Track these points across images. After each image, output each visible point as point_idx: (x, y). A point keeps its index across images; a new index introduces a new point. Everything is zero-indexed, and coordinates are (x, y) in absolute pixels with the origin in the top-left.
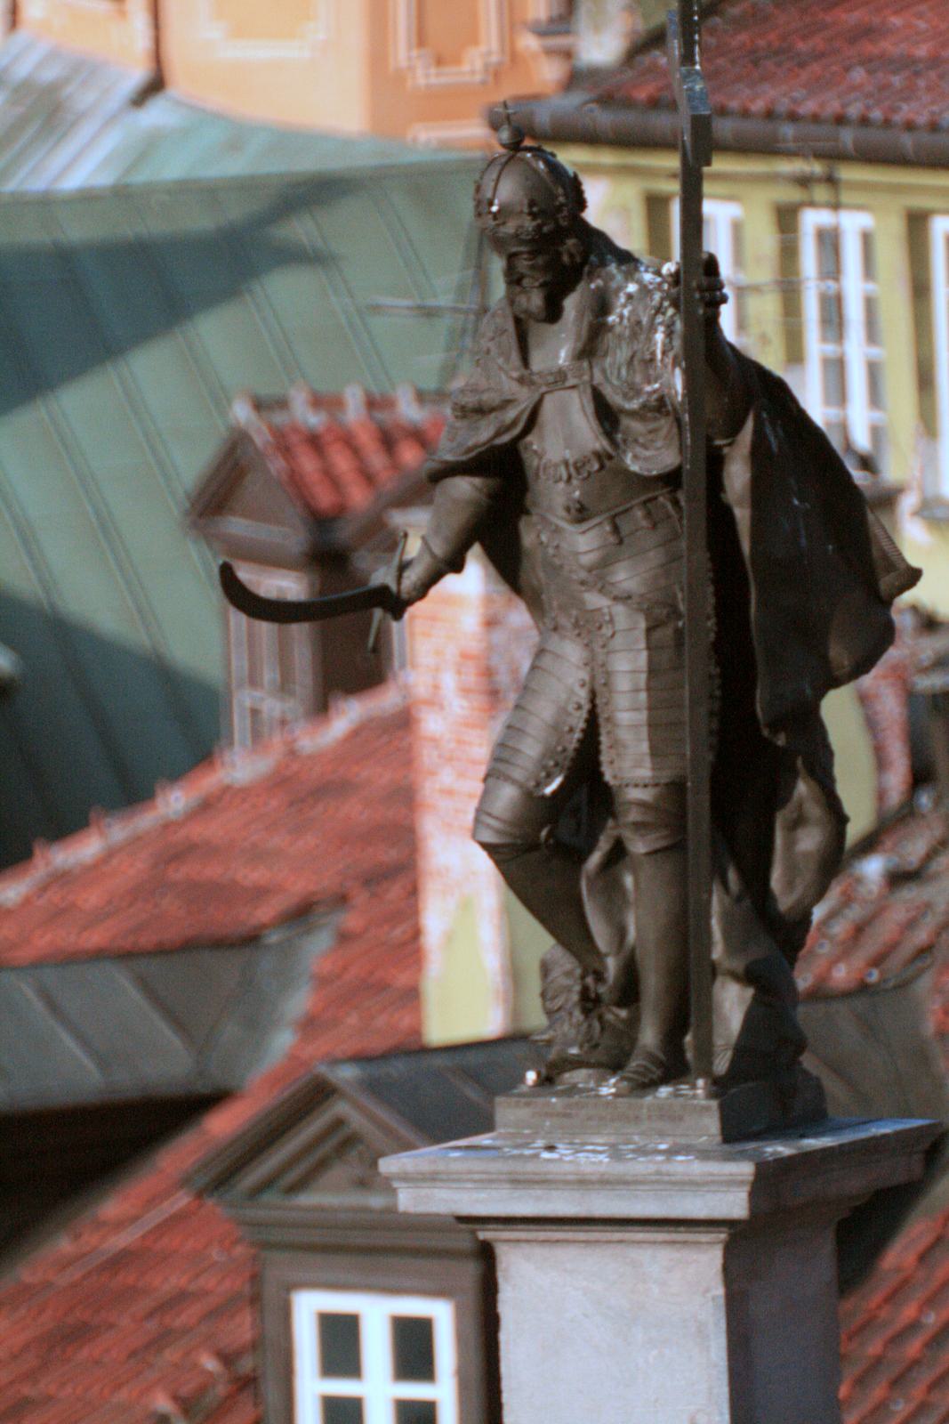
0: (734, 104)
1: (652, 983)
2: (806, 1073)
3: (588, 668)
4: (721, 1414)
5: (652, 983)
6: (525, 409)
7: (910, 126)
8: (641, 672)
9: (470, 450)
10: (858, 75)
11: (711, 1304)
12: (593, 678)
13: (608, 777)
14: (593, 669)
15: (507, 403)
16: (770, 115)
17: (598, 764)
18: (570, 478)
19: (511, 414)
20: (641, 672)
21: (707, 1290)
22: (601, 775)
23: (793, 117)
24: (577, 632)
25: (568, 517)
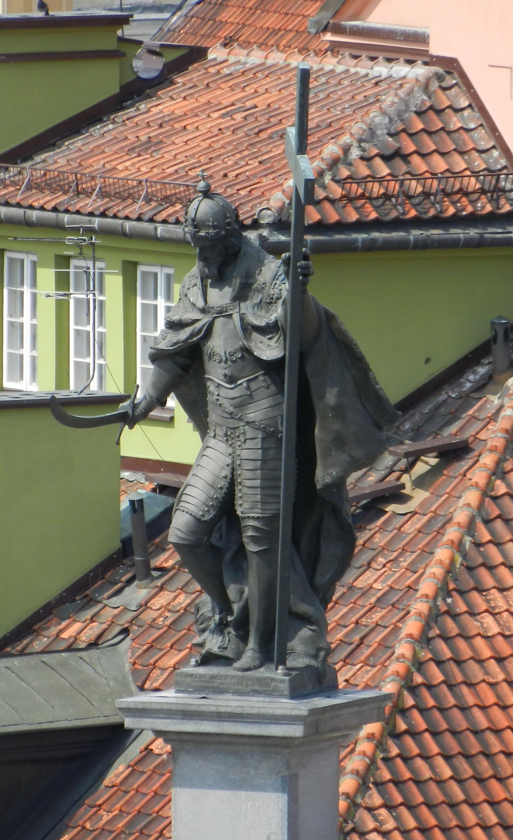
0: (36, 204)
1: (255, 617)
2: (300, 629)
3: (231, 457)
4: (283, 835)
5: (255, 617)
6: (205, 324)
7: (127, 218)
8: (259, 460)
9: (175, 344)
10: (415, 187)
11: (280, 780)
12: (233, 462)
13: (239, 513)
14: (233, 458)
15: (196, 321)
16: (55, 209)
17: (234, 505)
18: (227, 360)
19: (198, 325)
20: (259, 460)
21: (279, 772)
22: (235, 511)
23: (67, 211)
24: (225, 438)
25: (225, 380)
